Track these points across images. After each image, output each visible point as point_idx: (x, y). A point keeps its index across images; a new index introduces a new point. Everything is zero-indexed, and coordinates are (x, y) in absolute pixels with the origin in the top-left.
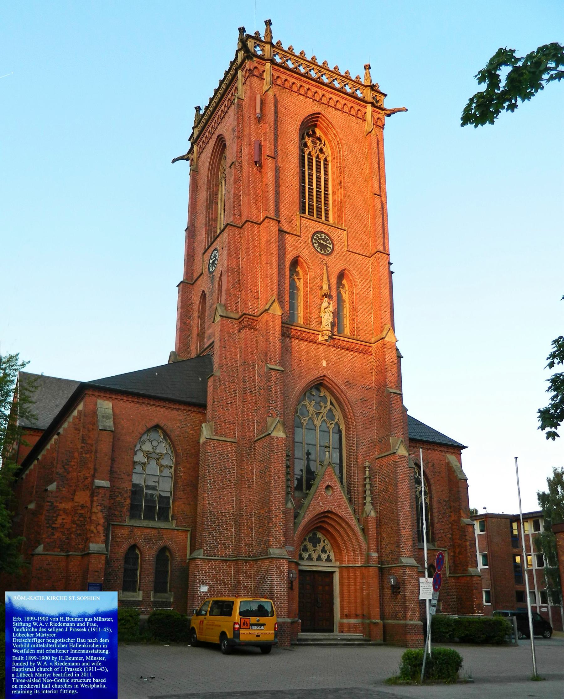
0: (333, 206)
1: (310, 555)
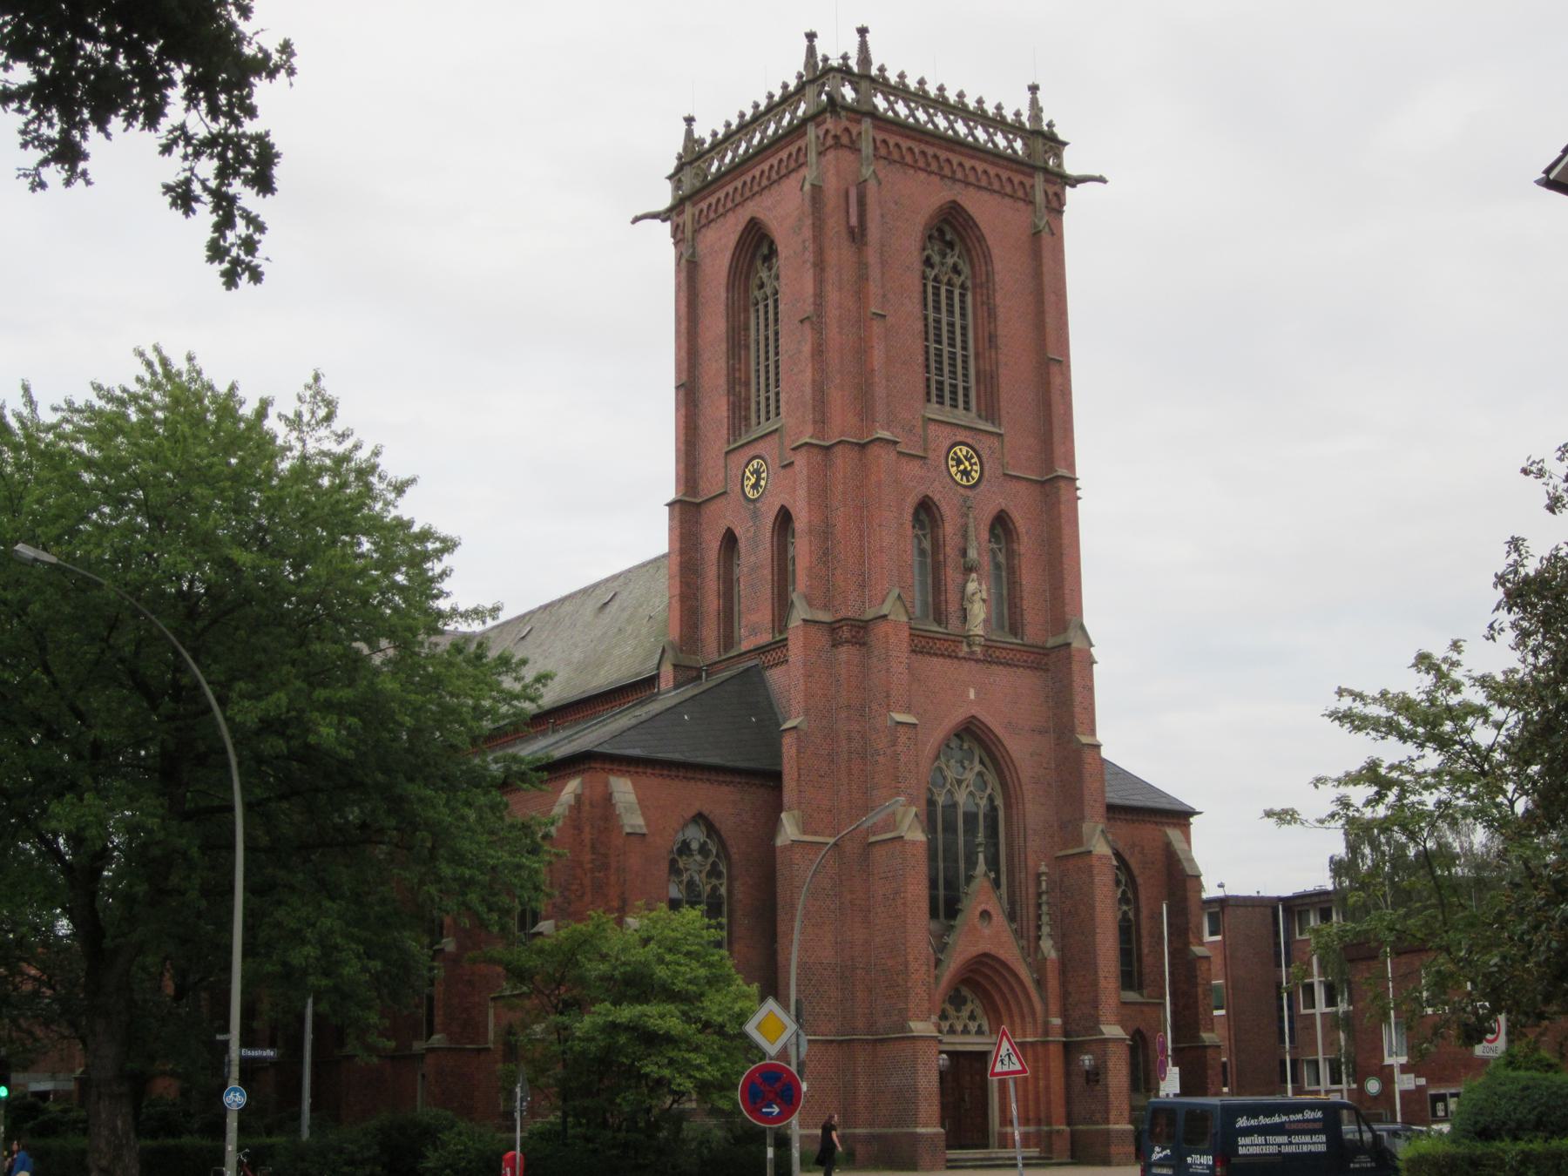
0: (978, 382)
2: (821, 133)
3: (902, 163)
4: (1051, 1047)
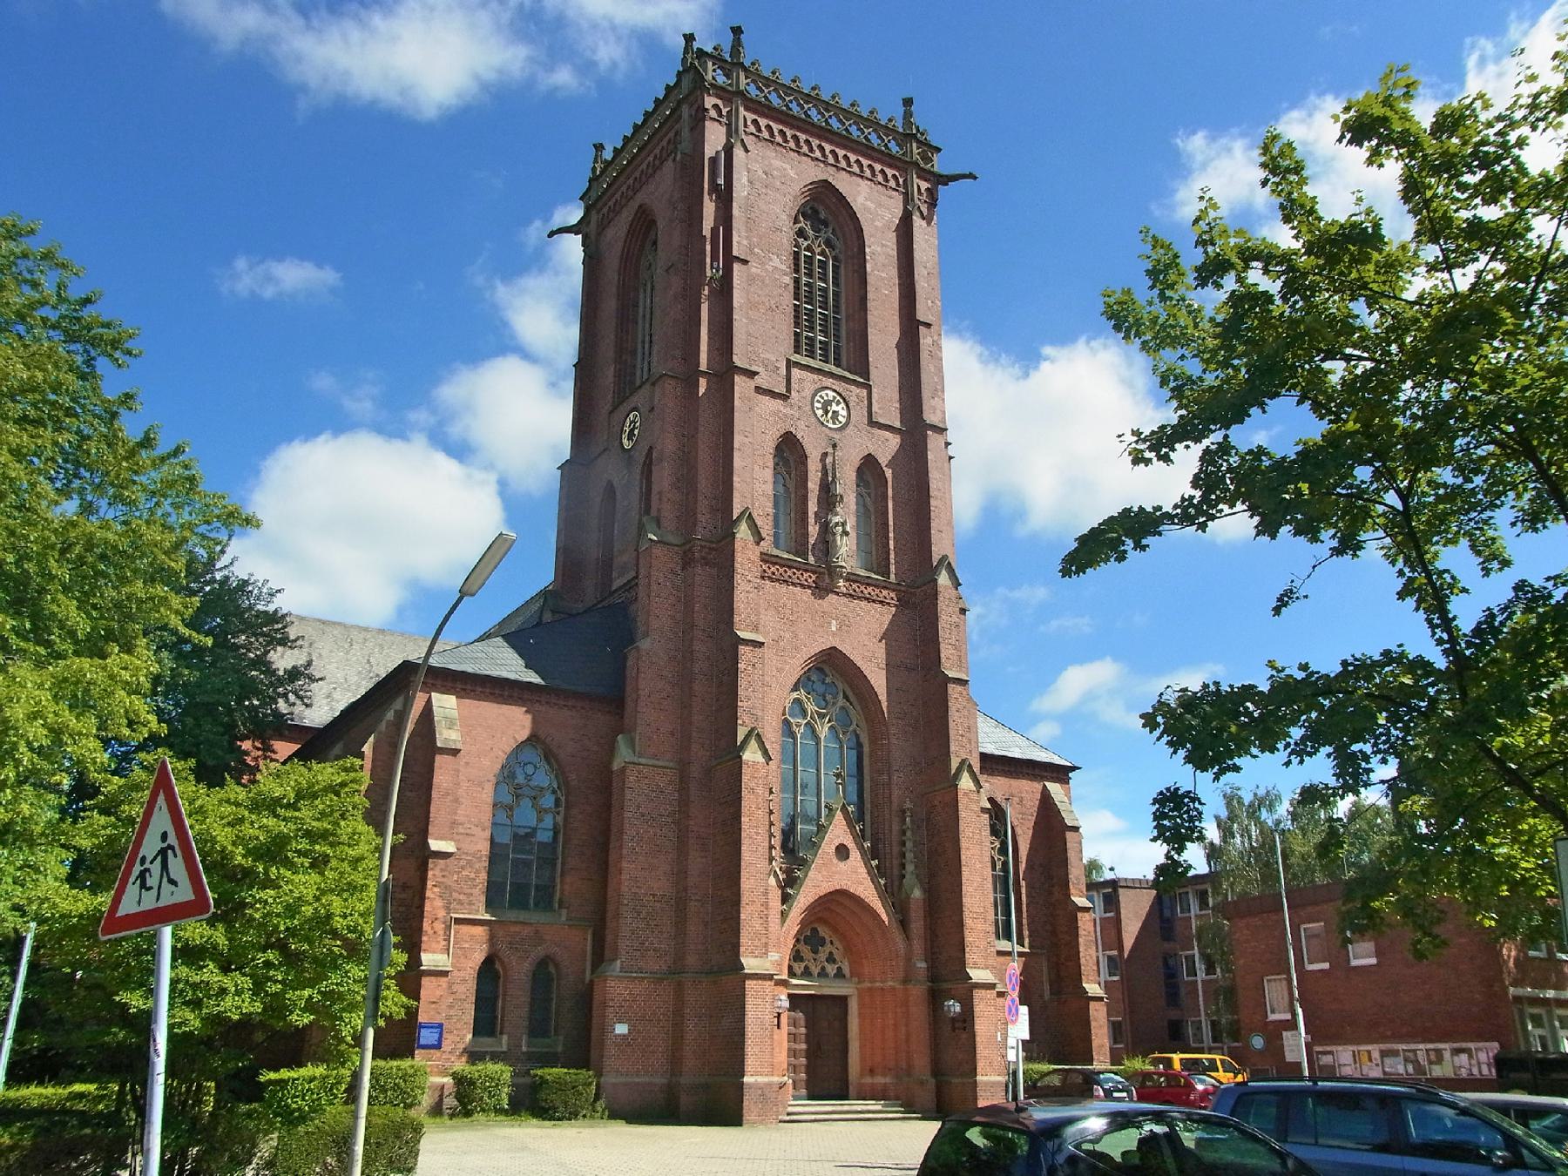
1: (806, 968)
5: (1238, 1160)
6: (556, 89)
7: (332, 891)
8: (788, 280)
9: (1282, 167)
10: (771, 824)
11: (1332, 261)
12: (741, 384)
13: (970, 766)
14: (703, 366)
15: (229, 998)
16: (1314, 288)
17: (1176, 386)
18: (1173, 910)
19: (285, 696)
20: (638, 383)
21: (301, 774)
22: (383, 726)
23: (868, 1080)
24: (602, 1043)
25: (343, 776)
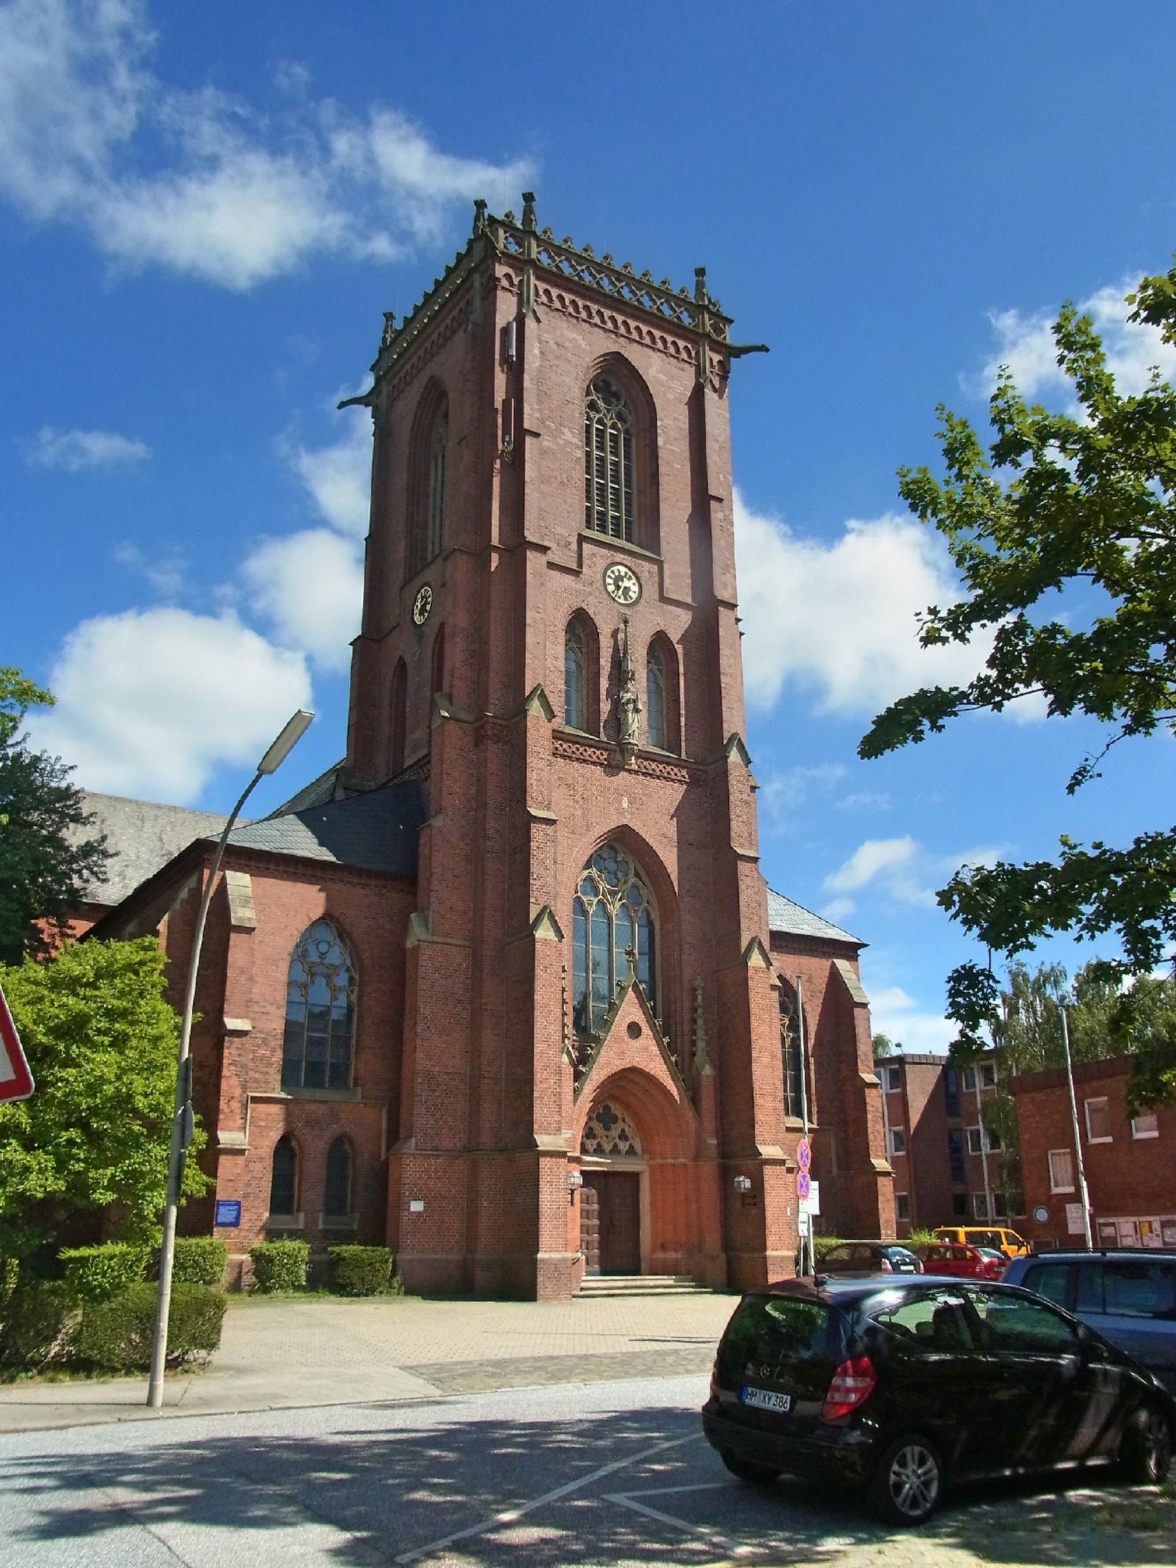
1: (599, 1144)
2: (485, 280)
3: (562, 311)
4: (241, 1135)
5: (1028, 1330)
6: (373, 255)
7: (132, 1069)
8: (580, 454)
9: (1077, 341)
10: (564, 1002)
11: (1129, 438)
12: (534, 561)
13: (760, 943)
14: (495, 540)
15: (33, 1176)
16: (1110, 467)
17: (973, 567)
18: (959, 1085)
19: (79, 872)
20: (429, 559)
21: (98, 953)
22: (177, 906)
23: (660, 1255)
24: (398, 1219)
25: (141, 956)
